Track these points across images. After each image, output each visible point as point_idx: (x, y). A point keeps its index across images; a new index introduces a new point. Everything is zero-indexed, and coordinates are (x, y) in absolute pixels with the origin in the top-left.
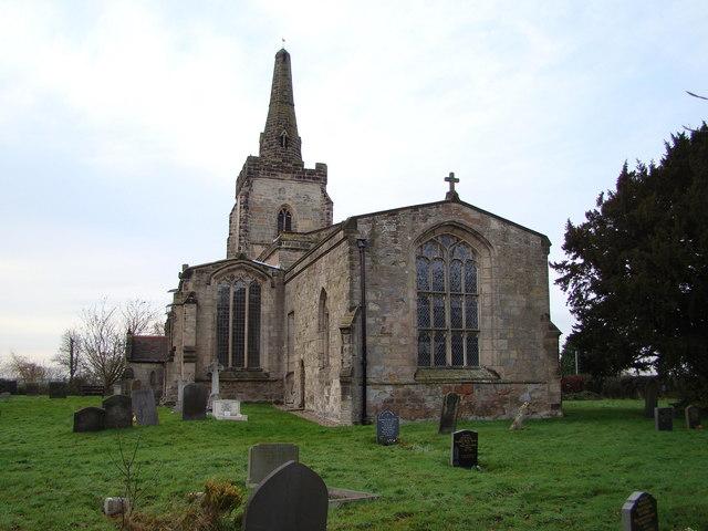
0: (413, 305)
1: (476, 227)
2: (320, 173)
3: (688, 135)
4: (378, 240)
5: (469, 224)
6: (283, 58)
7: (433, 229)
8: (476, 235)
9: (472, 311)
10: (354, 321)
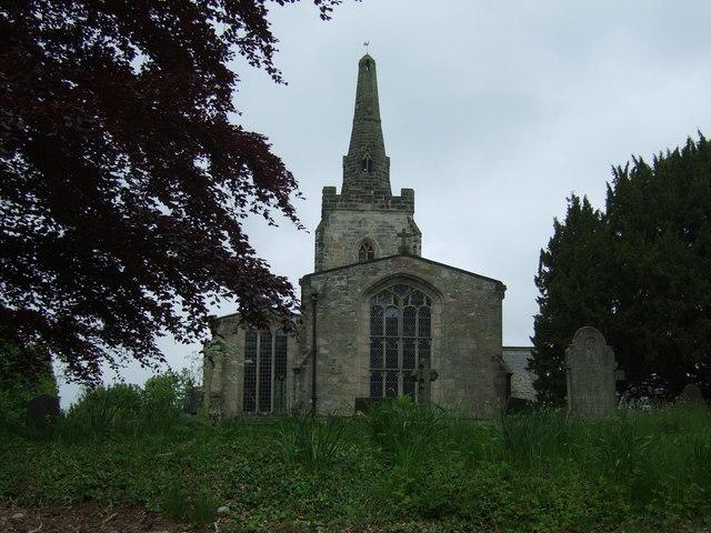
0: (367, 349)
1: (425, 277)
2: (407, 200)
3: (650, 163)
4: (329, 294)
5: (418, 274)
6: (367, 65)
7: (385, 281)
8: (427, 284)
9: (425, 346)
10: (305, 363)
